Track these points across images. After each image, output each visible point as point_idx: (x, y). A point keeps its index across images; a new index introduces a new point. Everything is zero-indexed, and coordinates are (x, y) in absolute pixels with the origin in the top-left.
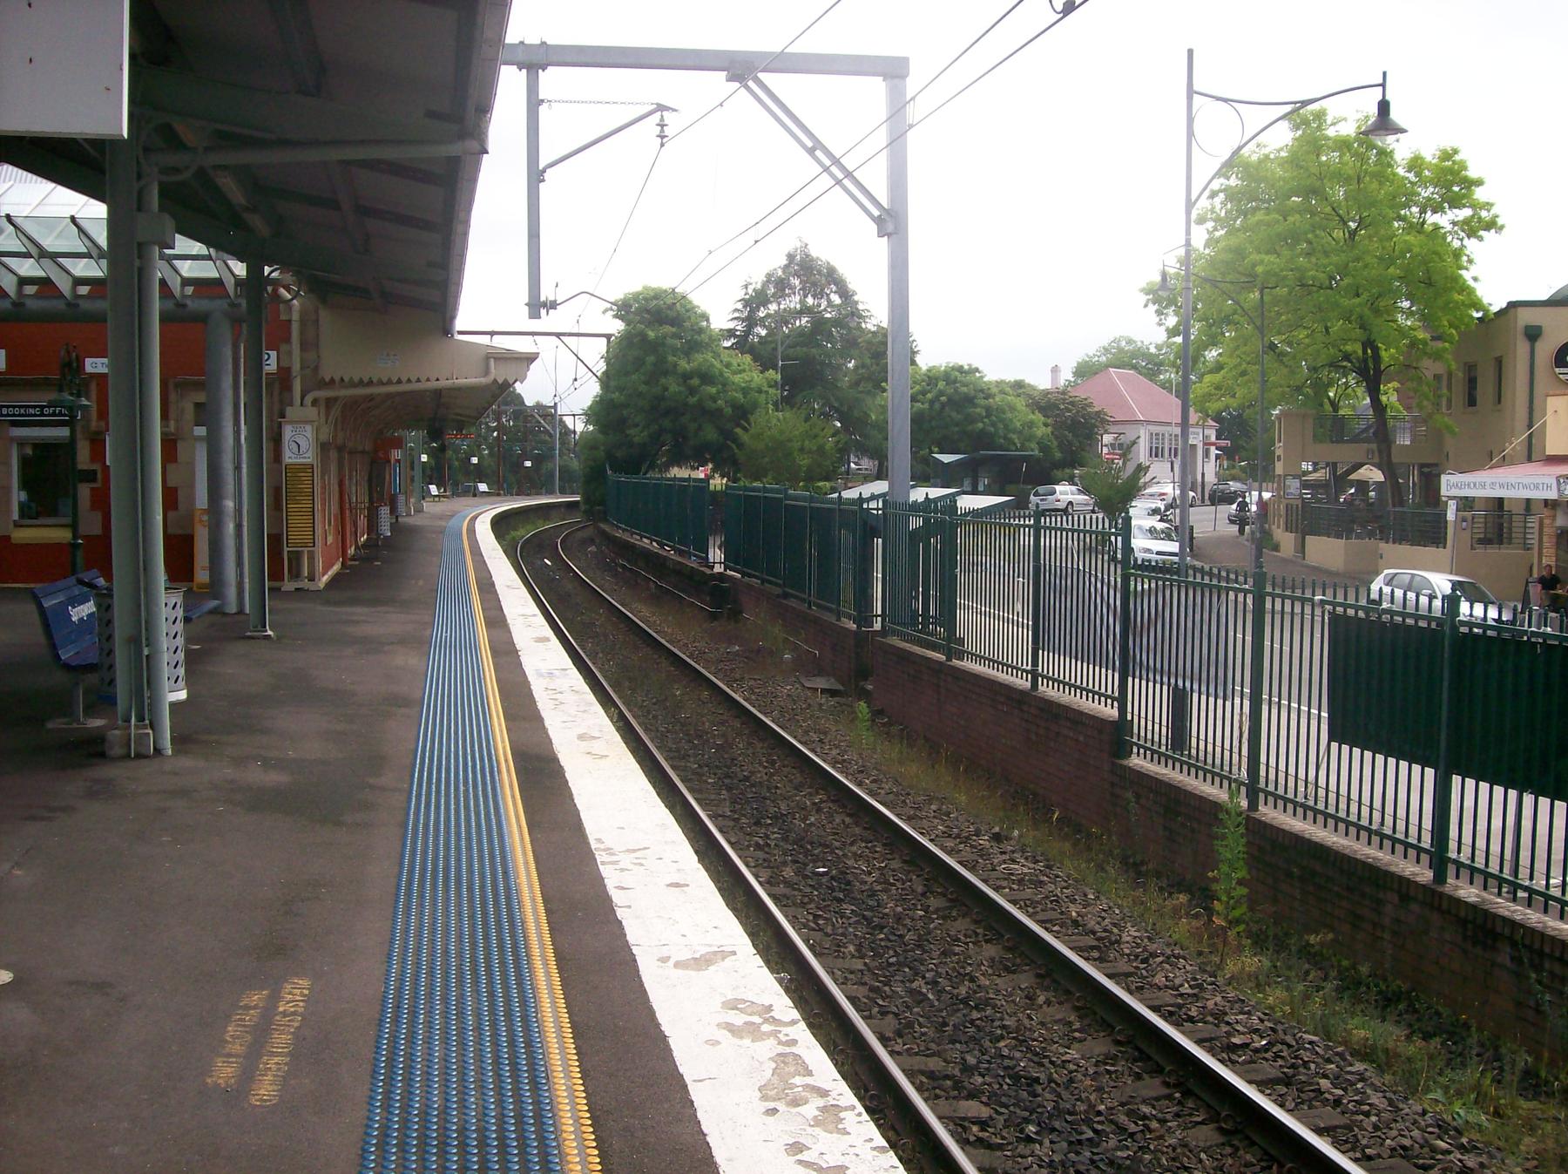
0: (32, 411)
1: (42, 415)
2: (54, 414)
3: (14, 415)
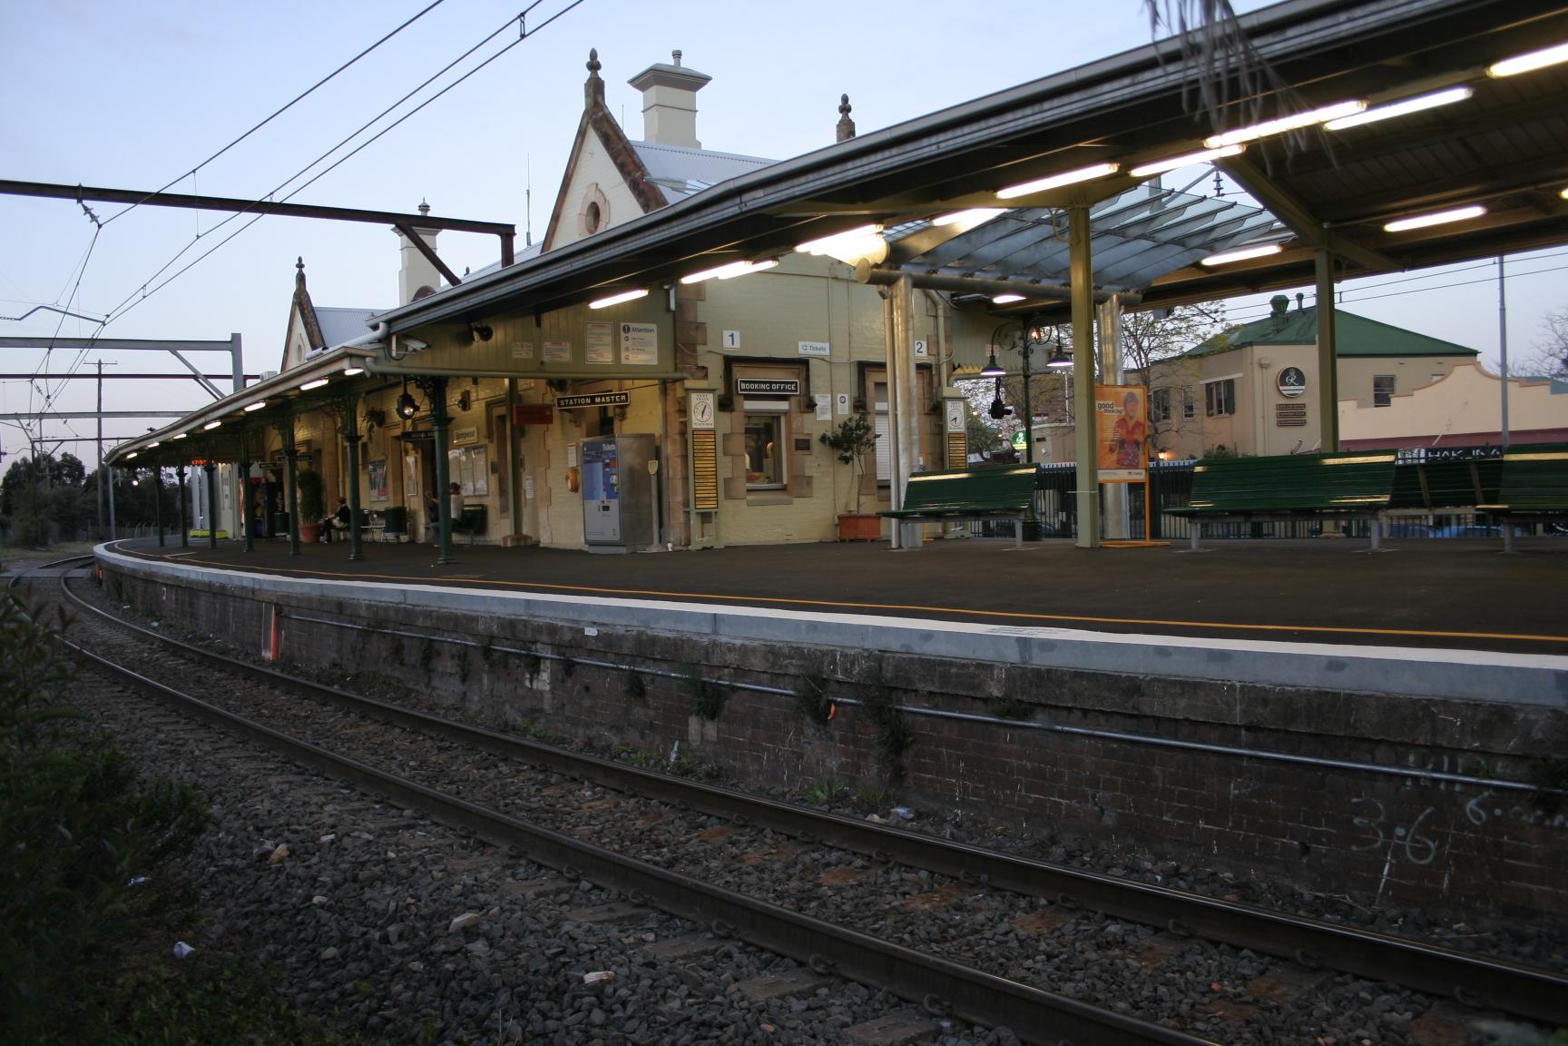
0: (763, 386)
1: (771, 390)
2: (779, 390)
3: (750, 390)
